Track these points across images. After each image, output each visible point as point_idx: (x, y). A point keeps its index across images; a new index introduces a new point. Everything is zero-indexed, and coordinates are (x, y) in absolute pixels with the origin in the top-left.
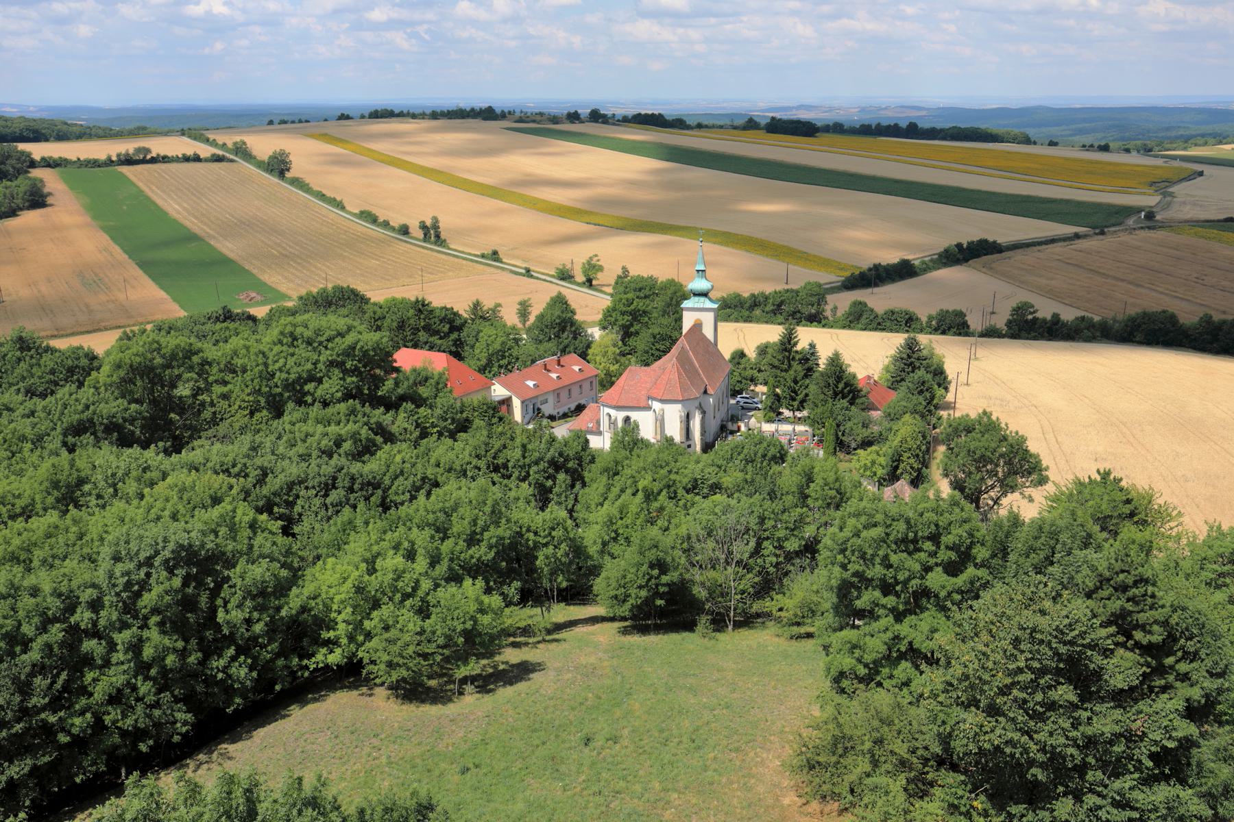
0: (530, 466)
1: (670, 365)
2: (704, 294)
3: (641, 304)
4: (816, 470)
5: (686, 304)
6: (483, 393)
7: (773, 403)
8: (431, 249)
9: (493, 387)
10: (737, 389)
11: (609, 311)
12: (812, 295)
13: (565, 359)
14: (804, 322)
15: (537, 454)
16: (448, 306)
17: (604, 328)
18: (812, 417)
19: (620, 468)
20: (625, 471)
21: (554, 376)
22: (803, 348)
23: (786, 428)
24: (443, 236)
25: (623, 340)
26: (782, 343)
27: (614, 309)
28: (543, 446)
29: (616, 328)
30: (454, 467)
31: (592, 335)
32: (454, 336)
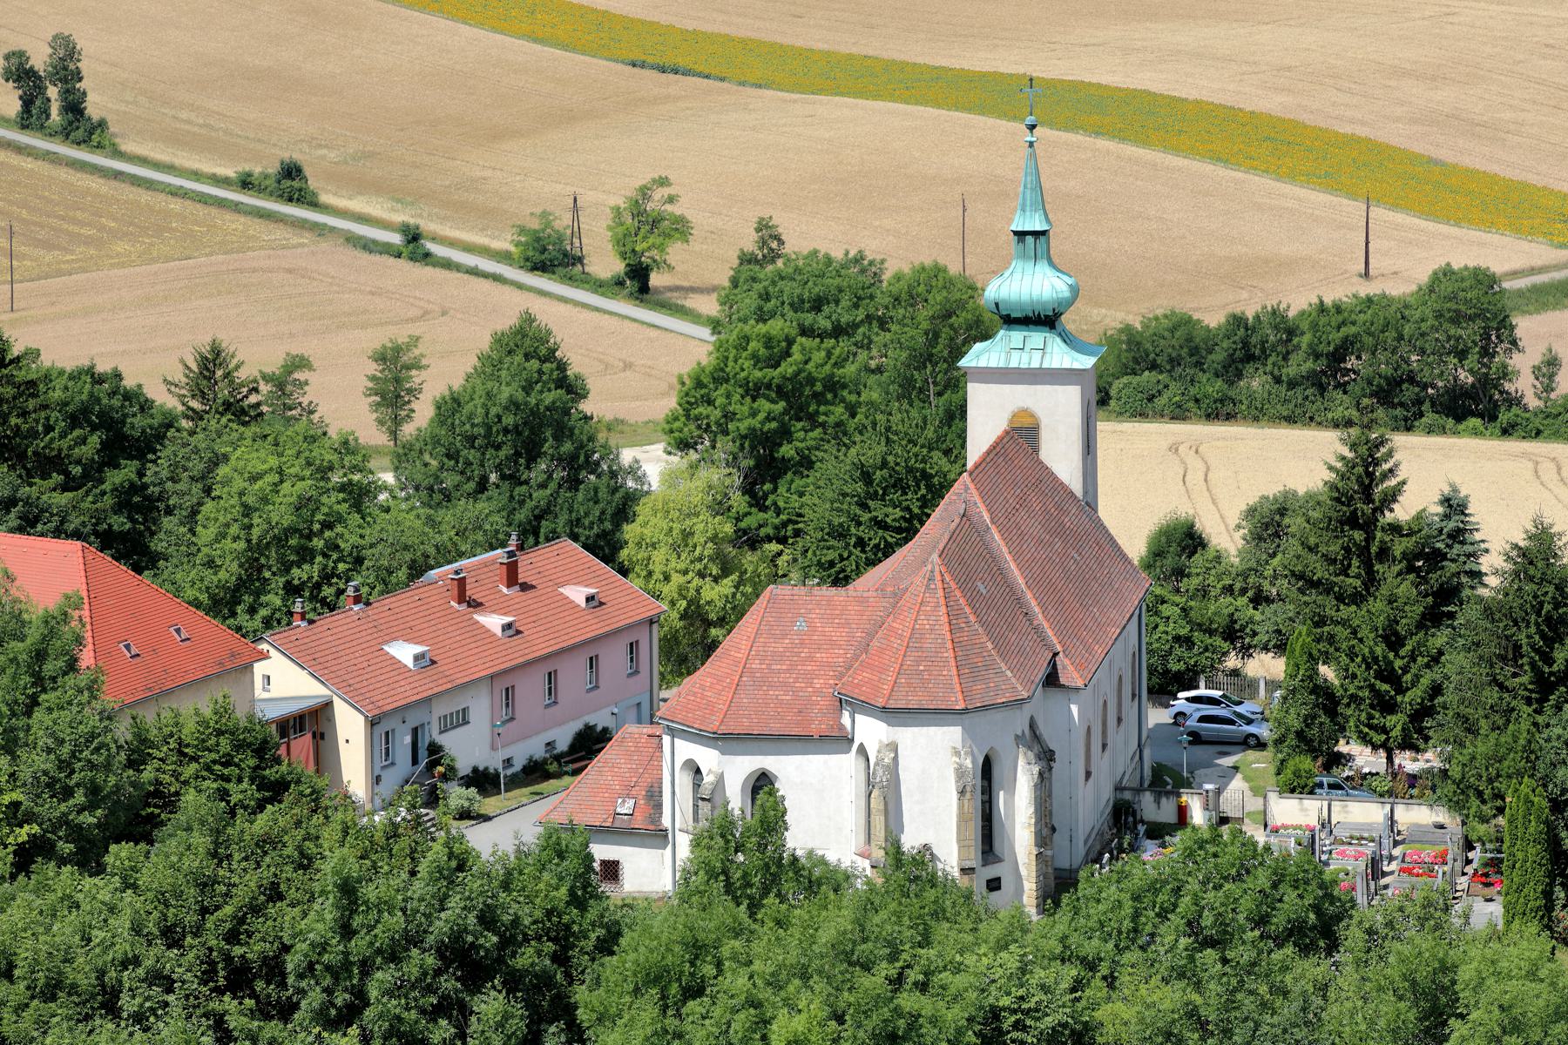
0: (366, 968)
1: (919, 581)
2: (1045, 319)
3: (819, 356)
4: (1465, 974)
5: (979, 356)
6: (218, 691)
7: (1309, 720)
8: (47, 156)
9: (260, 668)
10: (1175, 667)
11: (699, 384)
12: (1457, 318)
13: (537, 562)
14: (1430, 417)
15: (396, 921)
16: (103, 367)
17: (684, 445)
18: (1455, 772)
19: (709, 970)
20: (726, 981)
21: (493, 622)
22: (1419, 517)
23: (1363, 813)
24: (95, 107)
25: (748, 489)
26: (1339, 496)
27: (720, 376)
28: (418, 887)
29: (725, 445)
30: (71, 976)
31: (634, 470)
32: (122, 474)
